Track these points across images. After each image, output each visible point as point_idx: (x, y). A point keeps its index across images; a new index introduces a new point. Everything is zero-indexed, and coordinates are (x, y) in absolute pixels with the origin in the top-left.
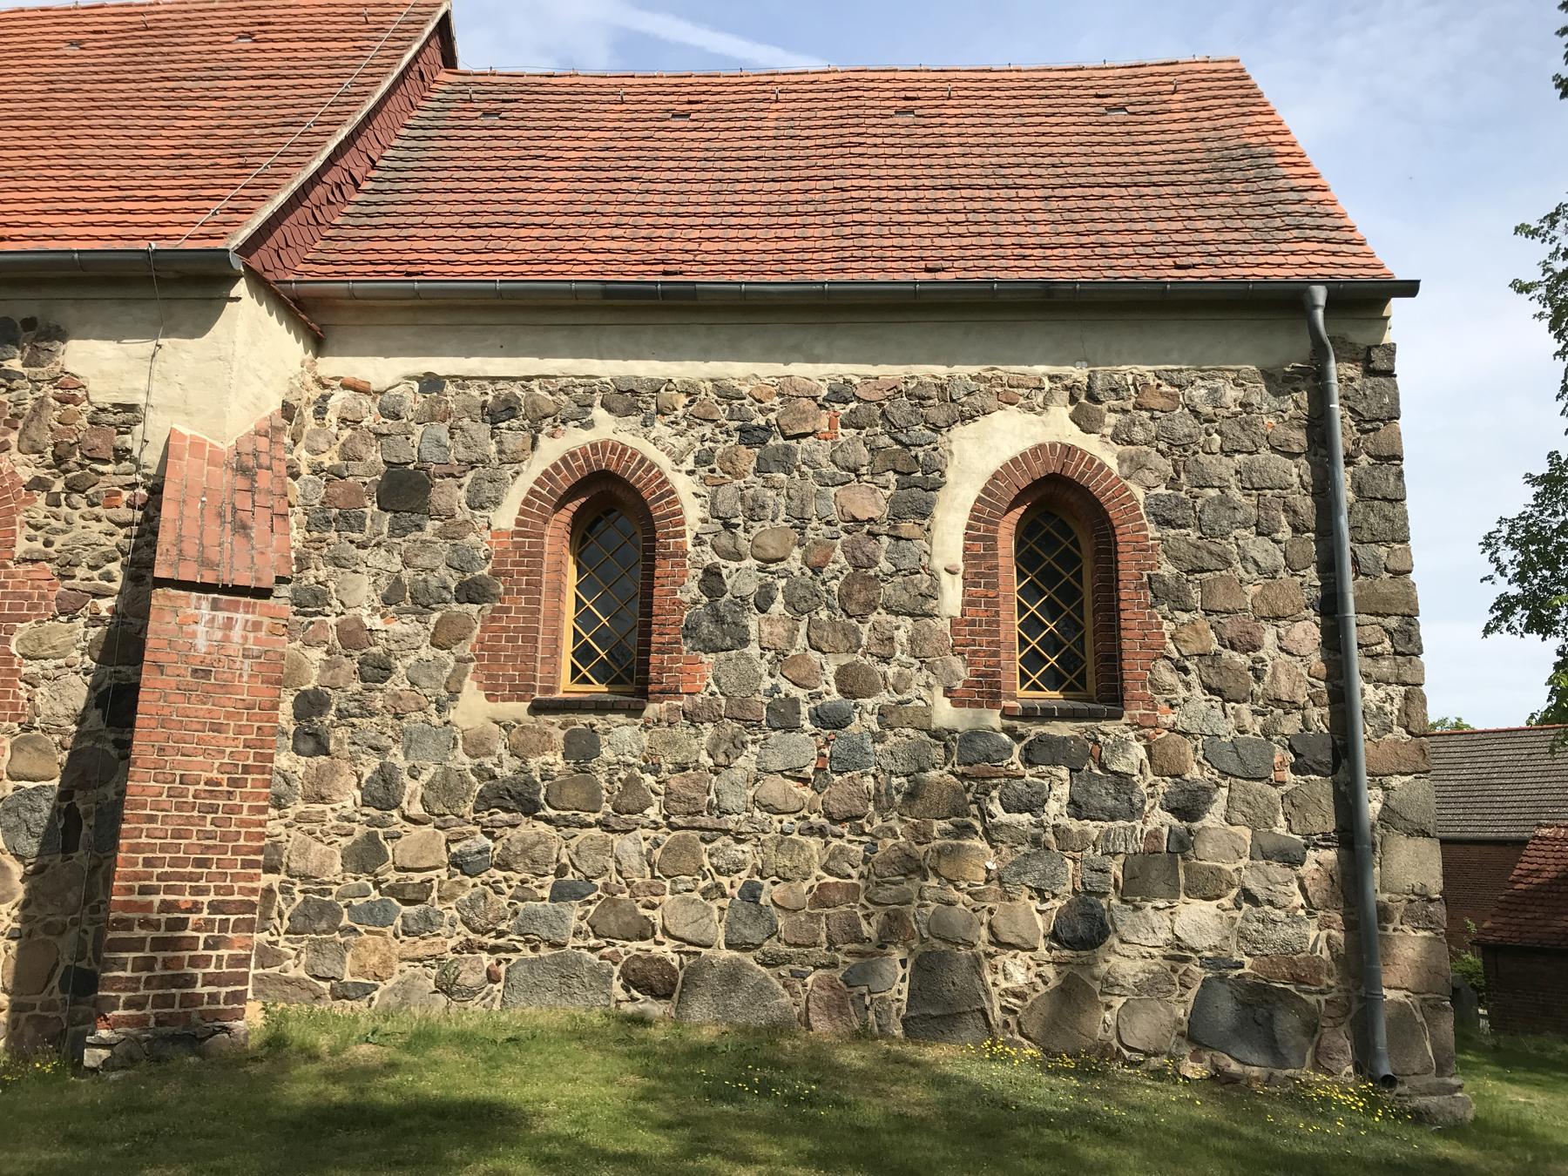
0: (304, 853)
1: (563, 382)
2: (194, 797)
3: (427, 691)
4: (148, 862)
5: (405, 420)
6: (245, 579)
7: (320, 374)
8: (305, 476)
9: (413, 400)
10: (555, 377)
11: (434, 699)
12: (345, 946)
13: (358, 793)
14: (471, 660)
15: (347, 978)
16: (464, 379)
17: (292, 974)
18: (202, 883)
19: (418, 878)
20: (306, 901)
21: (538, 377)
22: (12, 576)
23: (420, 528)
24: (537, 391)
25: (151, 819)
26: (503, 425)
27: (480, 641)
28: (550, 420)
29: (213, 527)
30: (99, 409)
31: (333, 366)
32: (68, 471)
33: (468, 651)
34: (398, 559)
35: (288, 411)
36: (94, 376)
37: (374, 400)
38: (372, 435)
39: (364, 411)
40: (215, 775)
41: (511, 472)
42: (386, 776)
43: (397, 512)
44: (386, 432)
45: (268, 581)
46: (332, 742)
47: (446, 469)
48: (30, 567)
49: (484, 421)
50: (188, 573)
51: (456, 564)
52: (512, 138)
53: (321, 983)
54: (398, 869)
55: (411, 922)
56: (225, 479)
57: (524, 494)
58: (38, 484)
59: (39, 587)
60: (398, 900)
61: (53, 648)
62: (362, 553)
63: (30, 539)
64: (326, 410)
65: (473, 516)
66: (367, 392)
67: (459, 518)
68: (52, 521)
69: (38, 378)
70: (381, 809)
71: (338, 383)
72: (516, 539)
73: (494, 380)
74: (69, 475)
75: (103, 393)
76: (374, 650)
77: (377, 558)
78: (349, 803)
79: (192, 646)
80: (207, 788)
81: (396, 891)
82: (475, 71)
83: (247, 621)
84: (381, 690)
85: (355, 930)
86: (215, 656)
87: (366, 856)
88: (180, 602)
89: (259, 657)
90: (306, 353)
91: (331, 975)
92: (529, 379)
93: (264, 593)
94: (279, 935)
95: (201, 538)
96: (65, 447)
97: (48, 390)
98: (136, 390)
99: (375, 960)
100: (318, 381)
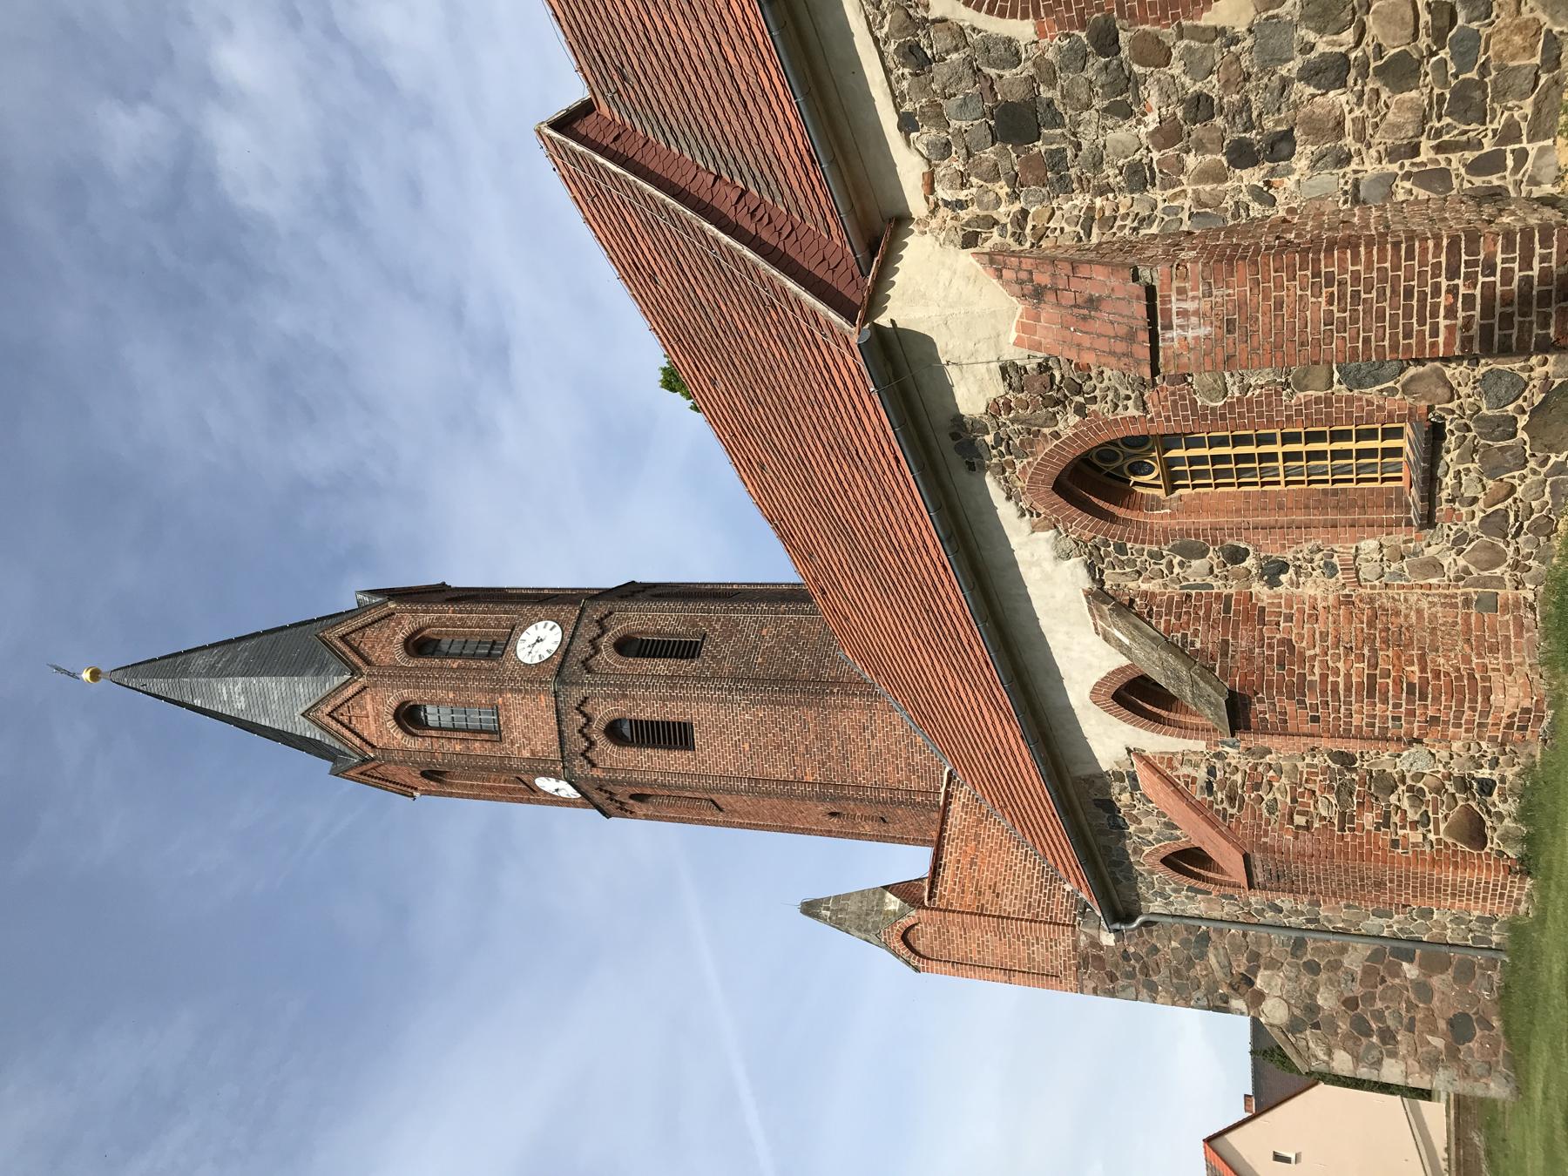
0: (1398, 127)
1: (869, 8)
2: (1345, 311)
3: (1218, 58)
4: (1408, 335)
5: (949, 137)
6: (1140, 309)
7: (927, 213)
8: (1023, 204)
9: (926, 135)
10: (867, 17)
11: (1225, 50)
12: (1501, 69)
13: (1332, 94)
14: (1179, 25)
15: (1537, 60)
16: (894, 97)
17: (1528, 109)
18: (1428, 290)
19: (1425, 17)
20: (1449, 114)
21: (872, 33)
22: (1158, 414)
23: (1050, 102)
24: (886, 29)
25: (1367, 340)
26: (929, 52)
27: (1157, 21)
28: (911, 11)
29: (1096, 326)
30: (1010, 388)
31: (917, 205)
32: (1066, 397)
33: (1170, 30)
34: (1085, 115)
35: (970, 241)
36: (985, 395)
37: (937, 166)
38: (971, 161)
39: (950, 171)
40: (1323, 300)
41: (975, 36)
42: (1311, 74)
43: (1039, 125)
44: (964, 151)
45: (1138, 289)
46: (1279, 129)
47: (987, 93)
48: (1150, 405)
49: (930, 71)
50: (1143, 352)
51: (1080, 64)
52: (639, 59)
53: (1542, 82)
54: (1415, 36)
55: (1476, 14)
56: (1048, 311)
57: (994, 19)
58: (1080, 410)
59: (1166, 397)
60: (1450, 30)
61: (1215, 381)
62: (1085, 145)
63: (1126, 408)
64: (958, 201)
65: (1028, 59)
66: (932, 173)
67: (1032, 71)
68: (1109, 399)
69: (995, 425)
70: (1349, 70)
71: (931, 197)
72: (1043, 15)
73: (887, 72)
74: (1068, 395)
75: (997, 389)
76: (1180, 114)
77: (1088, 136)
78: (1343, 98)
79: (1207, 337)
80: (1336, 303)
81: (1439, 37)
82: (586, 85)
83: (1178, 300)
84: (1221, 99)
85: (1483, 63)
86: (1213, 319)
87: (1401, 72)
88: (1170, 352)
89: (1210, 284)
90: (912, 231)
91: (1532, 76)
92: (876, 40)
93: (1150, 292)
94: (1487, 129)
95: (1110, 337)
96: (1046, 403)
97: (1003, 418)
98: (989, 370)
99: (1517, 39)
100: (933, 212)
